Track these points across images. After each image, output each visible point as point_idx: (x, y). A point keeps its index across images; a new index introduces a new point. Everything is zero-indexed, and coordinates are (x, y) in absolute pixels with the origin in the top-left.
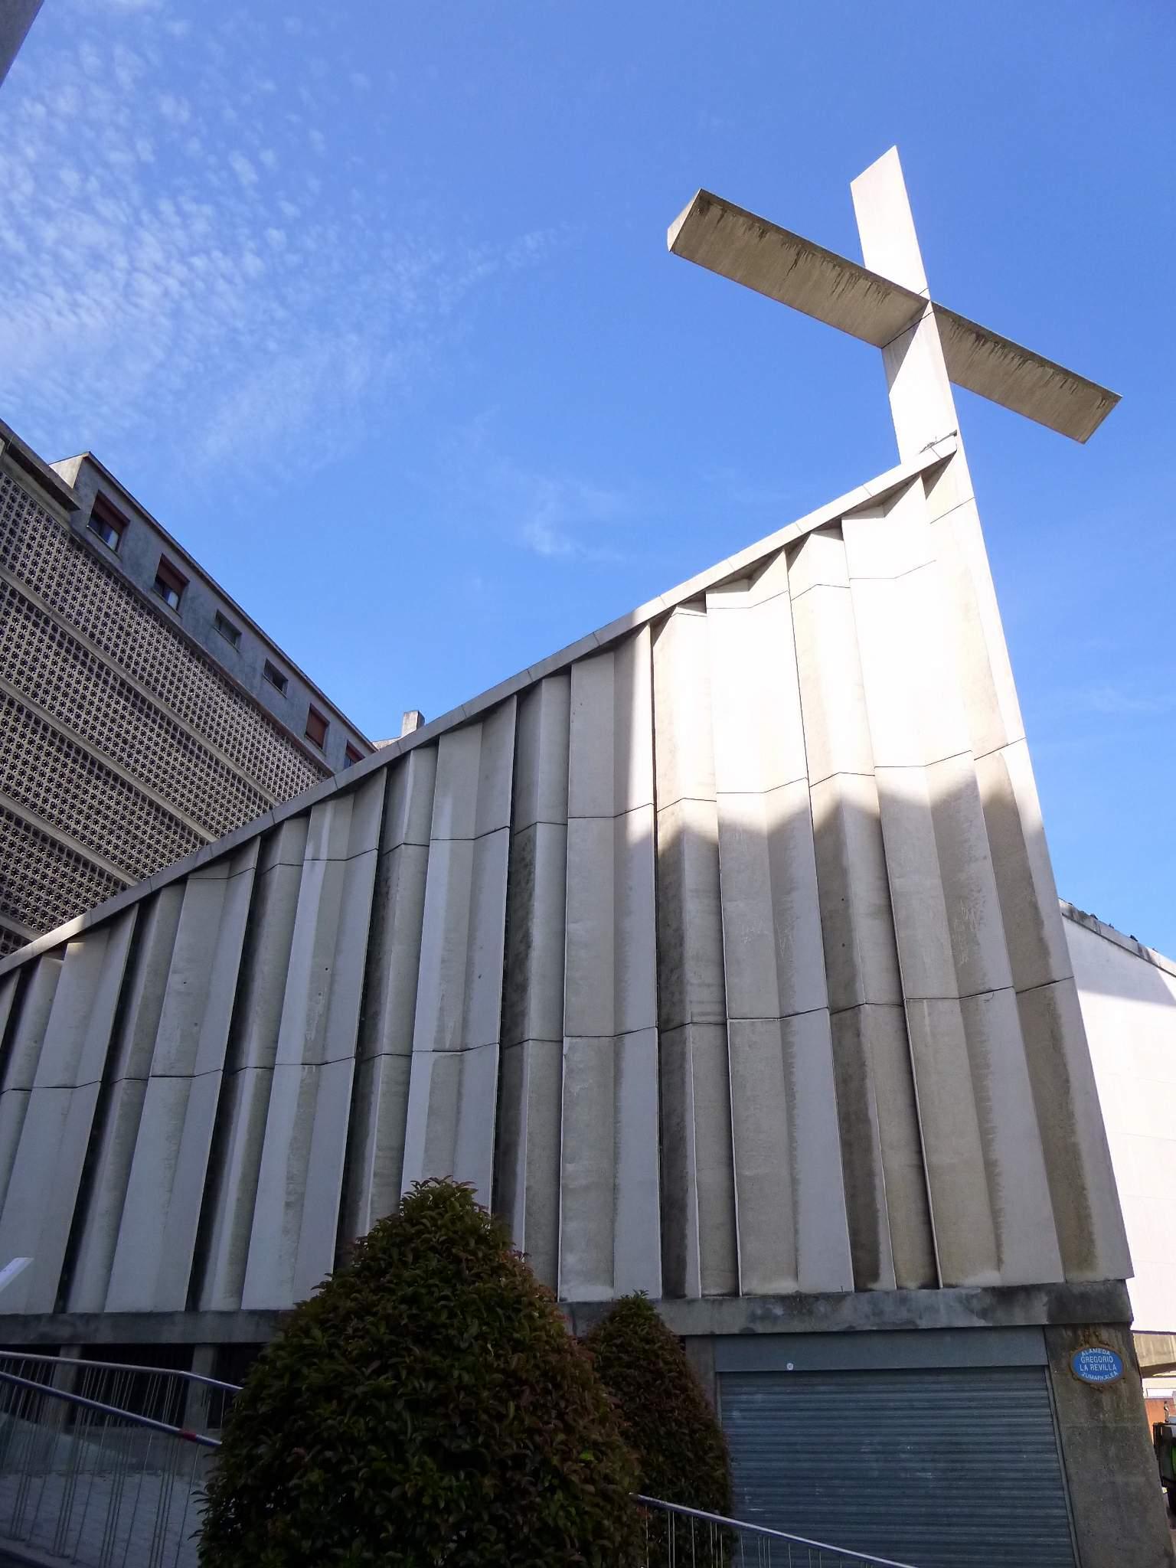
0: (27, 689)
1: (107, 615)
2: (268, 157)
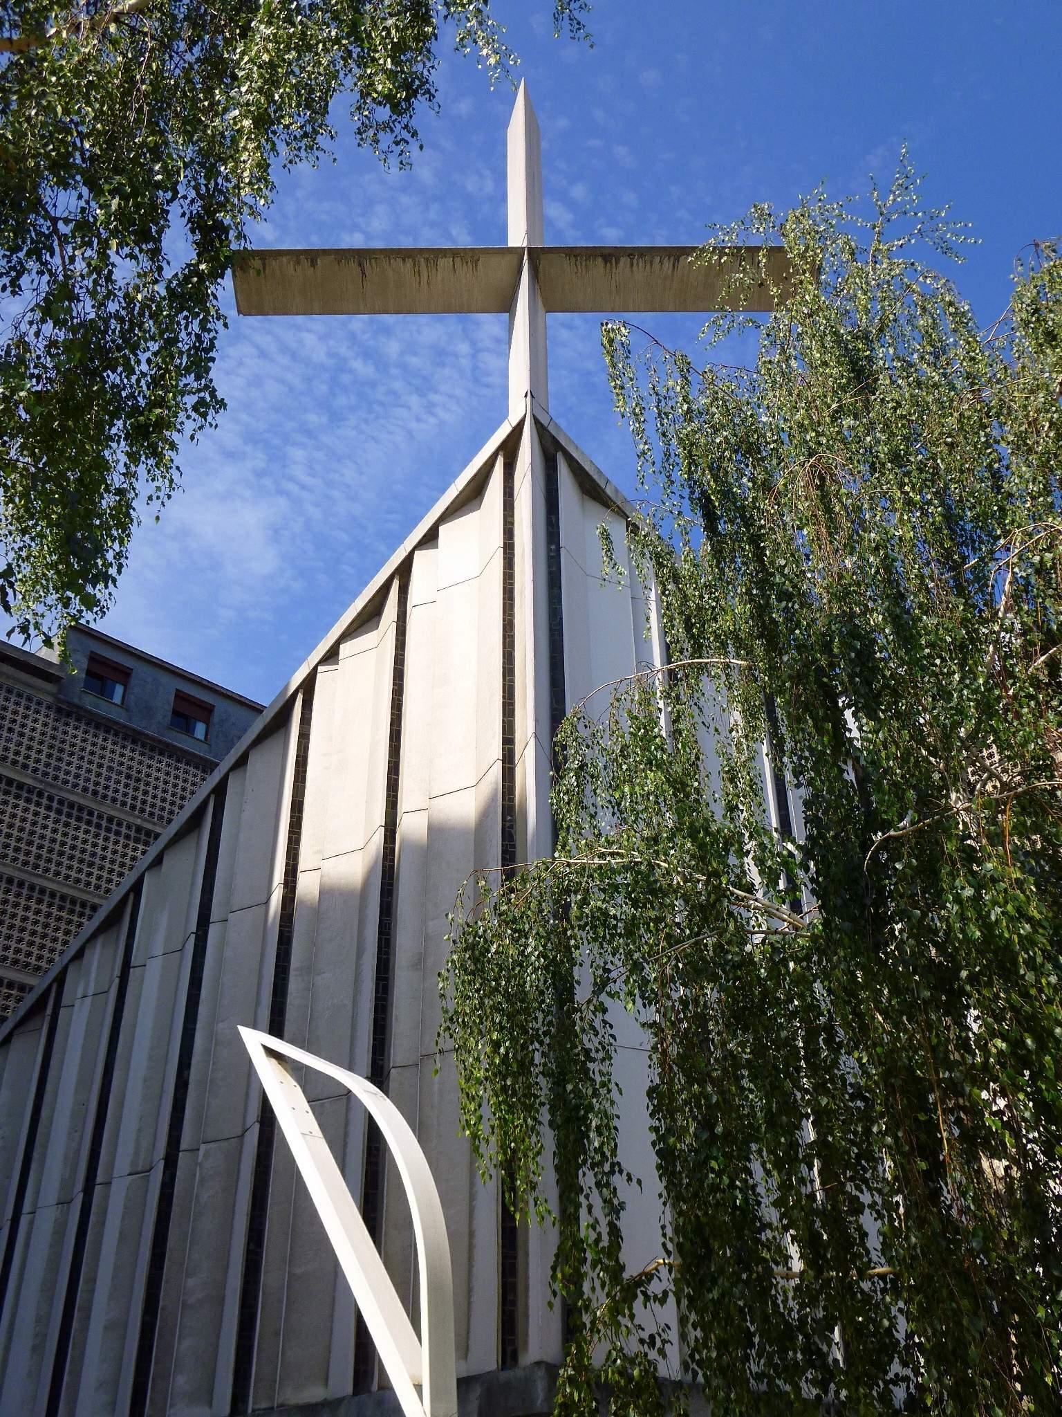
0: (26, 863)
1: (110, 769)
2: (579, 192)
